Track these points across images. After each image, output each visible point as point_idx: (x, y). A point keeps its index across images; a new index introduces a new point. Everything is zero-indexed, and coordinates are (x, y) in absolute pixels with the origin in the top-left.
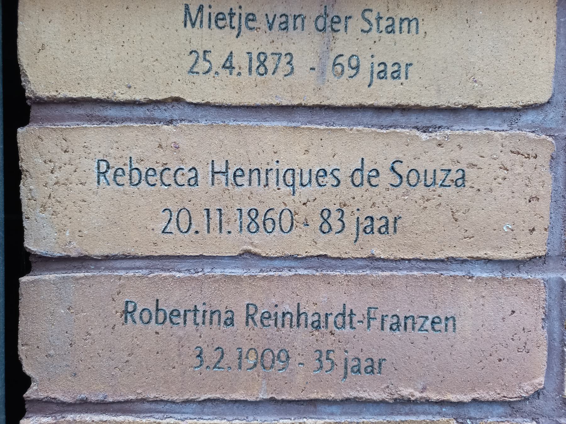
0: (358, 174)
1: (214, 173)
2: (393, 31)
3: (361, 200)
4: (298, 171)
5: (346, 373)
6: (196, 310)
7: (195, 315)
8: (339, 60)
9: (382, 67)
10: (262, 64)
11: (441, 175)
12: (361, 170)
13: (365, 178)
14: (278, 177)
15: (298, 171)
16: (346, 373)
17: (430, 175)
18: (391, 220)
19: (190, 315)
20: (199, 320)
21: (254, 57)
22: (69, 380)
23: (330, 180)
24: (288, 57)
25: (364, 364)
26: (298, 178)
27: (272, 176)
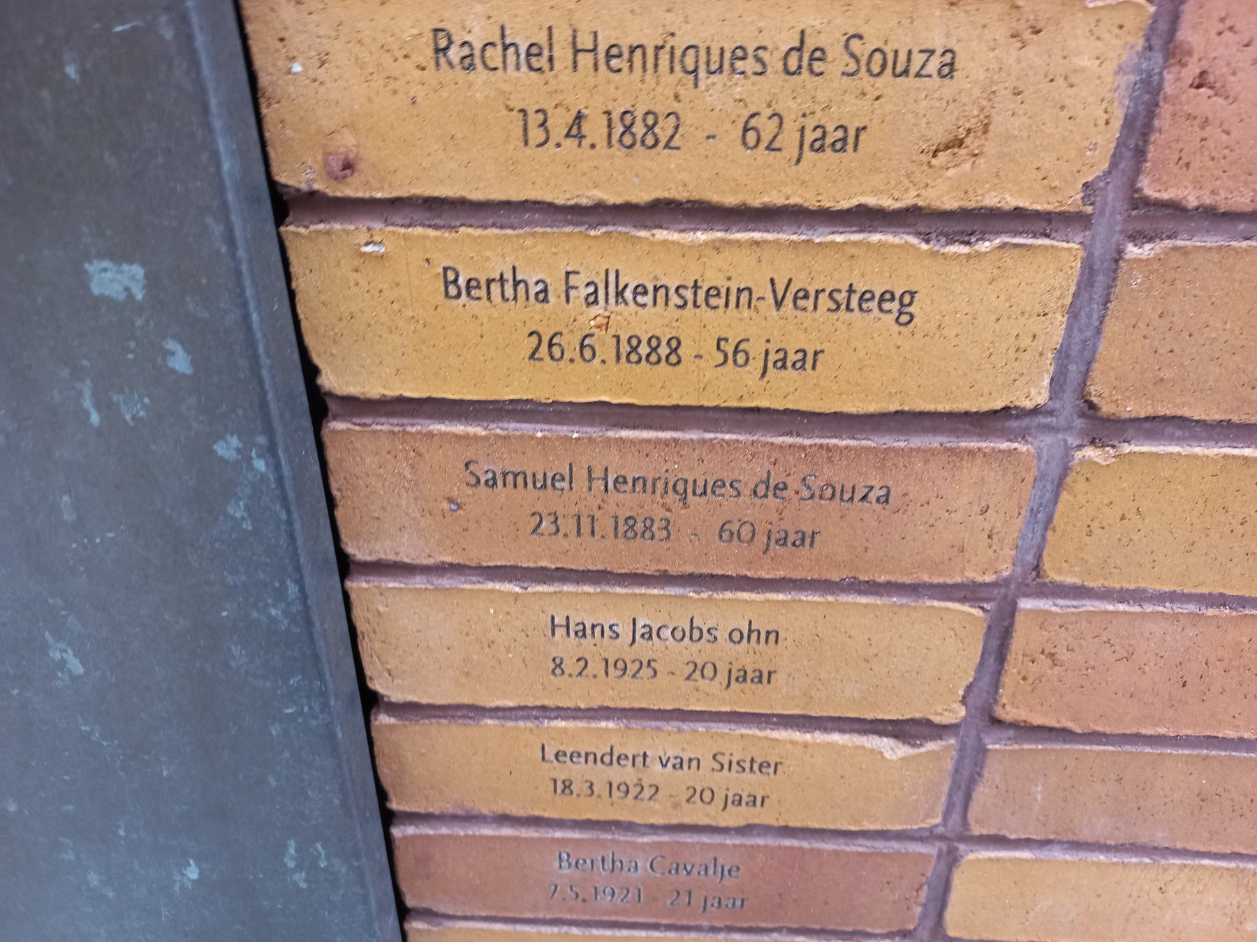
0: (795, 54)
1: (577, 51)
2: (843, 149)
3: (794, 98)
4: (530, 485)
5: (729, 683)
6: (502, 279)
7: (502, 286)
8: (753, 122)
10: (628, 129)
11: (918, 59)
12: (799, 49)
13: (805, 63)
14: (672, 62)
15: (530, 485)
16: (729, 683)
17: (902, 57)
18: (852, 133)
19: (495, 288)
20: (509, 291)
21: (621, 522)
22: (651, 171)
23: (750, 65)
24: (672, 119)
26: (703, 58)
27: (664, 57)
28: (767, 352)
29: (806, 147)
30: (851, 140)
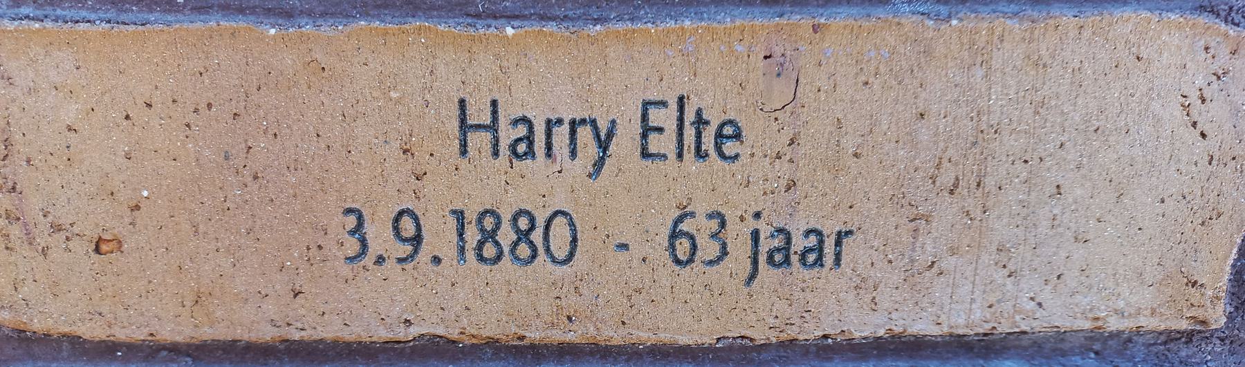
9: (812, 241)
10: (489, 236)
25: (799, 244)
28: (755, 235)
29: (762, 259)
30: (829, 249)
